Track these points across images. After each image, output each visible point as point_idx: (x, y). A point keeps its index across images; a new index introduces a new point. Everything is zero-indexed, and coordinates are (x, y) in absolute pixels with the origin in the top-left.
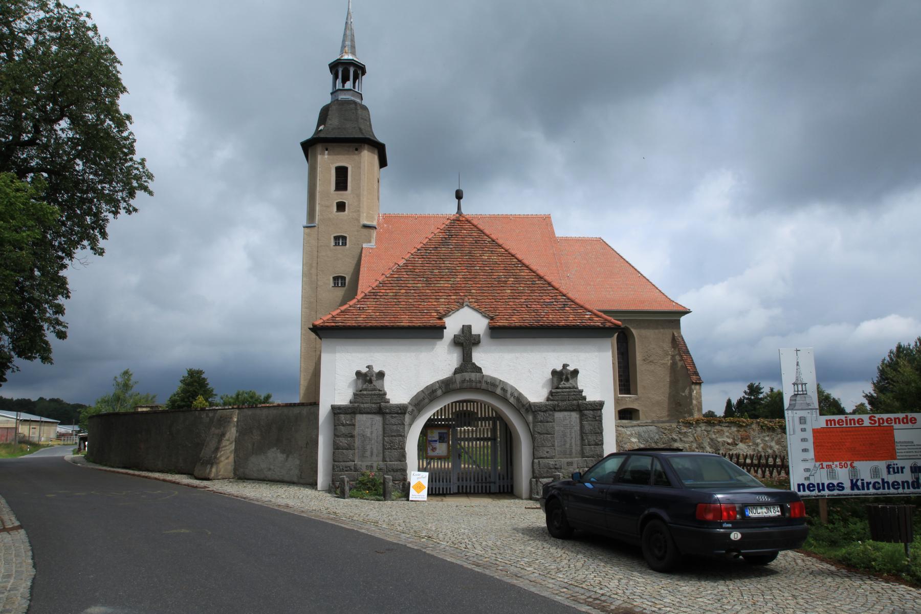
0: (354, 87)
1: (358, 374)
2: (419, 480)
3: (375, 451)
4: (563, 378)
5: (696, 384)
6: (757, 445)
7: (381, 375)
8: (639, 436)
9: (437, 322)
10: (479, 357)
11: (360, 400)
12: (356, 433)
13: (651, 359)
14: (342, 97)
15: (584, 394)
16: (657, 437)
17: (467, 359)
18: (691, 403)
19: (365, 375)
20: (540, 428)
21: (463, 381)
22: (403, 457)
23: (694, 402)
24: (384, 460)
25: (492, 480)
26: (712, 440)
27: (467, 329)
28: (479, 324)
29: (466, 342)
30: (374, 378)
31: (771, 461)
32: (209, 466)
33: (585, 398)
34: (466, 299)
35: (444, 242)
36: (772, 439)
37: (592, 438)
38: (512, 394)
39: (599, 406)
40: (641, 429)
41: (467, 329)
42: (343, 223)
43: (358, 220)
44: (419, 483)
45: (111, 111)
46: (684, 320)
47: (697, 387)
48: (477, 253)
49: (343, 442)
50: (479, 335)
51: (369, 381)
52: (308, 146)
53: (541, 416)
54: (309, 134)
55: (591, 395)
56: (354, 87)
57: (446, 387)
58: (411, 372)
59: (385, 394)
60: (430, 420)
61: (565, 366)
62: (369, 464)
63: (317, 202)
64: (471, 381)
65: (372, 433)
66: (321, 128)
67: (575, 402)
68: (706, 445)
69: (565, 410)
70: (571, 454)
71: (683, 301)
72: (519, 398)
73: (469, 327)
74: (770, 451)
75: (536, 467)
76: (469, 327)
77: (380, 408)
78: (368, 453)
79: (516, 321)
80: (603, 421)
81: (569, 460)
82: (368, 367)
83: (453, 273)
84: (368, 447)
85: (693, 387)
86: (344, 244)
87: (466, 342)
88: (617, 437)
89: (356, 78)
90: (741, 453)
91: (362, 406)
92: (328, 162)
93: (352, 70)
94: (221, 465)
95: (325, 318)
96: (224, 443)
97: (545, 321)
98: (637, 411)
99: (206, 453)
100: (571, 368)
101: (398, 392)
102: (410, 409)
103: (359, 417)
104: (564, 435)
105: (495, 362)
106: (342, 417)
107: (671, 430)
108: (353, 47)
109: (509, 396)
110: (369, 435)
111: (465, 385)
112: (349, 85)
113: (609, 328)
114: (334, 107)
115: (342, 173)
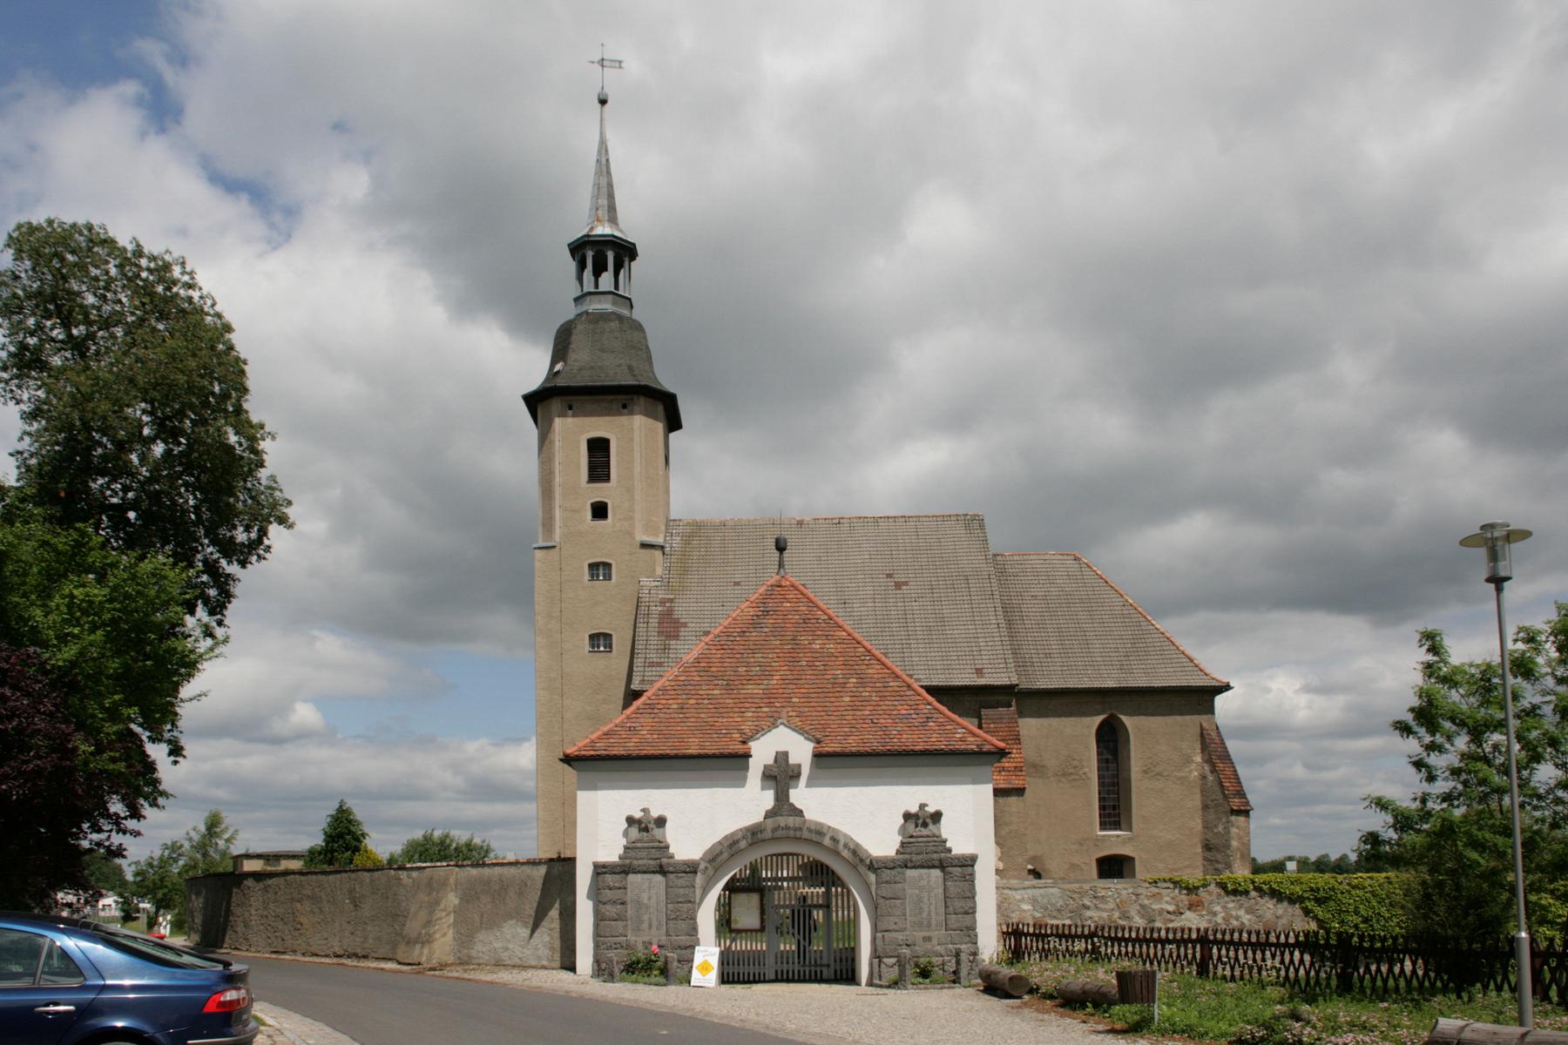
0: (617, 287)
1: (631, 821)
2: (707, 955)
3: (655, 923)
4: (922, 821)
5: (1238, 812)
6: (1215, 914)
7: (661, 822)
8: (1034, 901)
9: (739, 748)
10: (800, 795)
11: (632, 854)
12: (628, 898)
13: (1157, 770)
14: (595, 306)
15: (948, 845)
16: (1061, 902)
17: (782, 798)
18: (1228, 846)
19: (639, 822)
20: (886, 890)
21: (775, 830)
22: (693, 930)
23: (1234, 843)
24: (668, 934)
25: (825, 961)
26: (1142, 906)
27: (782, 757)
28: (801, 751)
29: (781, 776)
30: (651, 826)
31: (1219, 936)
32: (418, 946)
33: (950, 850)
34: (784, 714)
35: (755, 623)
36: (1241, 906)
37: (958, 904)
38: (846, 846)
39: (969, 862)
40: (1037, 892)
41: (782, 757)
42: (604, 539)
43: (631, 535)
44: (706, 962)
45: (239, 417)
46: (1220, 701)
47: (1242, 819)
48: (804, 639)
49: (611, 910)
50: (799, 766)
51: (645, 827)
52: (535, 401)
53: (887, 875)
54: (535, 381)
55: (959, 846)
56: (617, 287)
57: (754, 834)
59: (667, 847)
60: (733, 879)
61: (922, 806)
62: (647, 939)
63: (557, 503)
64: (787, 828)
66: (558, 367)
68: (1133, 913)
69: (922, 867)
70: (929, 925)
71: (1218, 672)
72: (856, 851)
73: (786, 754)
74: (1235, 923)
75: (879, 942)
76: (786, 754)
79: (852, 744)
80: (977, 882)
81: (927, 934)
82: (643, 810)
83: (766, 674)
84: (646, 917)
85: (1233, 818)
86: (608, 577)
87: (781, 776)
88: (999, 907)
89: (618, 266)
90: (1189, 925)
92: (575, 432)
93: (610, 256)
94: (436, 945)
95: (581, 744)
96: (439, 914)
97: (895, 744)
98: (1131, 859)
99: (413, 927)
100: (931, 809)
101: (686, 844)
102: (702, 866)
103: (631, 877)
104: (920, 900)
105: (820, 803)
106: (609, 878)
107: (1083, 894)
108: (612, 209)
109: (841, 846)
110: (101, 904)
111: (779, 834)
112: (606, 280)
113: (989, 753)
114: (580, 327)
115: (598, 448)
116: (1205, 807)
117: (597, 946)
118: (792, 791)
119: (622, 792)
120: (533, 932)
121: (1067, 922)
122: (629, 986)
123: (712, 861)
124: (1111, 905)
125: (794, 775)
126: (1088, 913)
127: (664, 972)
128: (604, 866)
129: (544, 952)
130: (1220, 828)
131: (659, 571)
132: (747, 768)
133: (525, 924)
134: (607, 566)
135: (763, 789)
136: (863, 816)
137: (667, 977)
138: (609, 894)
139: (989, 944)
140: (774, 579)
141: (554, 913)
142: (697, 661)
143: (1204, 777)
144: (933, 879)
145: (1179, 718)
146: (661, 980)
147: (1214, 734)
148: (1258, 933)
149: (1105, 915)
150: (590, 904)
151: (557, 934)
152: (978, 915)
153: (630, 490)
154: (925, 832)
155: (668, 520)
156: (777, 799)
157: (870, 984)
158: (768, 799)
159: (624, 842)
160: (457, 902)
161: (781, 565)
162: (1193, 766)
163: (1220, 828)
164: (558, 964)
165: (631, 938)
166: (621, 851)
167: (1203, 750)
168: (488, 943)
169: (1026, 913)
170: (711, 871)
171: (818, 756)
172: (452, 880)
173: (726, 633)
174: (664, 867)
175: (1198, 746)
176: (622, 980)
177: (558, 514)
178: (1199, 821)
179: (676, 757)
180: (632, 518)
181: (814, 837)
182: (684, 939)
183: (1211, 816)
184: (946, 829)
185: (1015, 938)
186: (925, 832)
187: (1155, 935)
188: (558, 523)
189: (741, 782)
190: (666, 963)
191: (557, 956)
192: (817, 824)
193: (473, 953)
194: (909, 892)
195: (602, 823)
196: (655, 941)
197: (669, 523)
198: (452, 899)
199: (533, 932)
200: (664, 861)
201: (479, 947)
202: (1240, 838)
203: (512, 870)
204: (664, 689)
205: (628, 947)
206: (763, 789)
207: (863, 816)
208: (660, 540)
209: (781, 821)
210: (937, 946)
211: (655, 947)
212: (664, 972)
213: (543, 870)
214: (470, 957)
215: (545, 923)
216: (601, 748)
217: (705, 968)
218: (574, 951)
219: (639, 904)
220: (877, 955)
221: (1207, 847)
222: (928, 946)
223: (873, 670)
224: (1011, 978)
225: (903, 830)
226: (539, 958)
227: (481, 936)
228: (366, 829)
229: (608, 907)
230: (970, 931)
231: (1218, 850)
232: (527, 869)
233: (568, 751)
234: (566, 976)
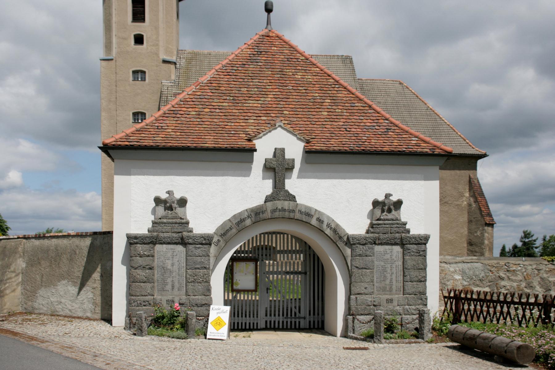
1: (158, 201)
2: (220, 313)
3: (177, 285)
4: (387, 207)
8: (463, 273)
10: (294, 184)
11: (159, 228)
12: (155, 264)
17: (279, 186)
18: (483, 243)
19: (165, 202)
20: (359, 262)
21: (274, 211)
23: (486, 242)
24: (187, 294)
25: (302, 314)
27: (279, 153)
28: (295, 149)
30: (175, 205)
33: (408, 231)
35: (251, 59)
37: (414, 274)
38: (328, 225)
39: (423, 241)
40: (466, 266)
41: (279, 153)
42: (142, 57)
43: (157, 54)
44: (219, 318)
47: (490, 228)
48: (289, 72)
49: (141, 274)
51: (170, 207)
53: (360, 249)
57: (257, 215)
58: (216, 200)
59: (188, 223)
60: (236, 252)
61: (388, 196)
62: (170, 298)
64: (283, 210)
65: (173, 265)
67: (397, 235)
68: (535, 284)
69: (387, 244)
70: (391, 290)
72: (336, 230)
73: (283, 150)
75: (353, 303)
76: (283, 150)
77: (182, 238)
78: (169, 287)
79: (334, 144)
82: (168, 192)
84: (169, 280)
85: (486, 228)
86: (143, 79)
87: (278, 168)
91: (161, 235)
95: (117, 137)
96: (9, 275)
97: (367, 146)
100: (394, 198)
101: (203, 220)
102: (215, 239)
103: (158, 247)
104: (384, 270)
109: (325, 226)
110: (169, 267)
111: (277, 214)
113: (439, 155)
116: (470, 221)
117: (129, 303)
118: (287, 181)
119: (151, 177)
120: (80, 289)
121: (487, 289)
122: (155, 338)
123: (223, 235)
124: (520, 277)
125: (290, 168)
126: (503, 283)
127: (185, 326)
128: (136, 237)
129: (88, 306)
130: (479, 233)
131: (173, 77)
132: (251, 161)
133: (74, 284)
134: (144, 72)
135: (264, 178)
136: (342, 201)
137: (187, 331)
138: (140, 261)
139: (435, 306)
140: (264, 32)
141: (96, 275)
142: (210, 82)
143: (470, 205)
144: (395, 254)
145: (458, 172)
146: (182, 333)
147: (476, 181)
148: (455, 291)
149: (515, 284)
150: (124, 268)
151: (98, 292)
152: (428, 283)
153: (157, 28)
154: (390, 216)
155: (178, 51)
156: (275, 186)
157: (345, 335)
158: (267, 187)
159: (152, 218)
160: (24, 265)
161: (268, 22)
162: (464, 199)
163: (479, 233)
164: (99, 316)
165: (157, 297)
166: (150, 225)
167: (470, 190)
168: (46, 298)
169: (459, 282)
170: (222, 243)
171: (308, 152)
172: (20, 249)
173: (231, 64)
174: (184, 239)
175: (467, 188)
176: (150, 333)
177: (114, 40)
178: (466, 229)
179: (196, 149)
180: (157, 45)
181: (304, 218)
182: (200, 299)
183: (473, 227)
184: (405, 214)
185: (457, 302)
186: (390, 216)
187: (469, 296)
188: (114, 45)
189: (247, 172)
190: (186, 319)
191: (98, 310)
192: (306, 207)
193: (36, 305)
194: (376, 263)
195: (133, 201)
196: (177, 300)
197: (179, 52)
198: (21, 264)
199: (80, 289)
200: (185, 234)
201: (40, 300)
202: (489, 239)
203: (65, 241)
204: (185, 101)
205: (155, 304)
206: (264, 178)
207: (342, 201)
208: (174, 59)
209: (279, 204)
210: (395, 305)
211: (177, 304)
212: (185, 326)
213: (88, 241)
214: (34, 308)
215: (90, 283)
216: (134, 141)
217: (219, 323)
218: (111, 306)
219: (164, 269)
220: (349, 312)
221: (470, 244)
222: (390, 306)
223: (343, 94)
224: (519, 348)
225: (371, 214)
226: (85, 311)
227: (42, 292)
228: (9, 225)
229: (139, 271)
230: (422, 295)
231: (476, 245)
232: (76, 241)
233: (107, 141)
234: (103, 327)
